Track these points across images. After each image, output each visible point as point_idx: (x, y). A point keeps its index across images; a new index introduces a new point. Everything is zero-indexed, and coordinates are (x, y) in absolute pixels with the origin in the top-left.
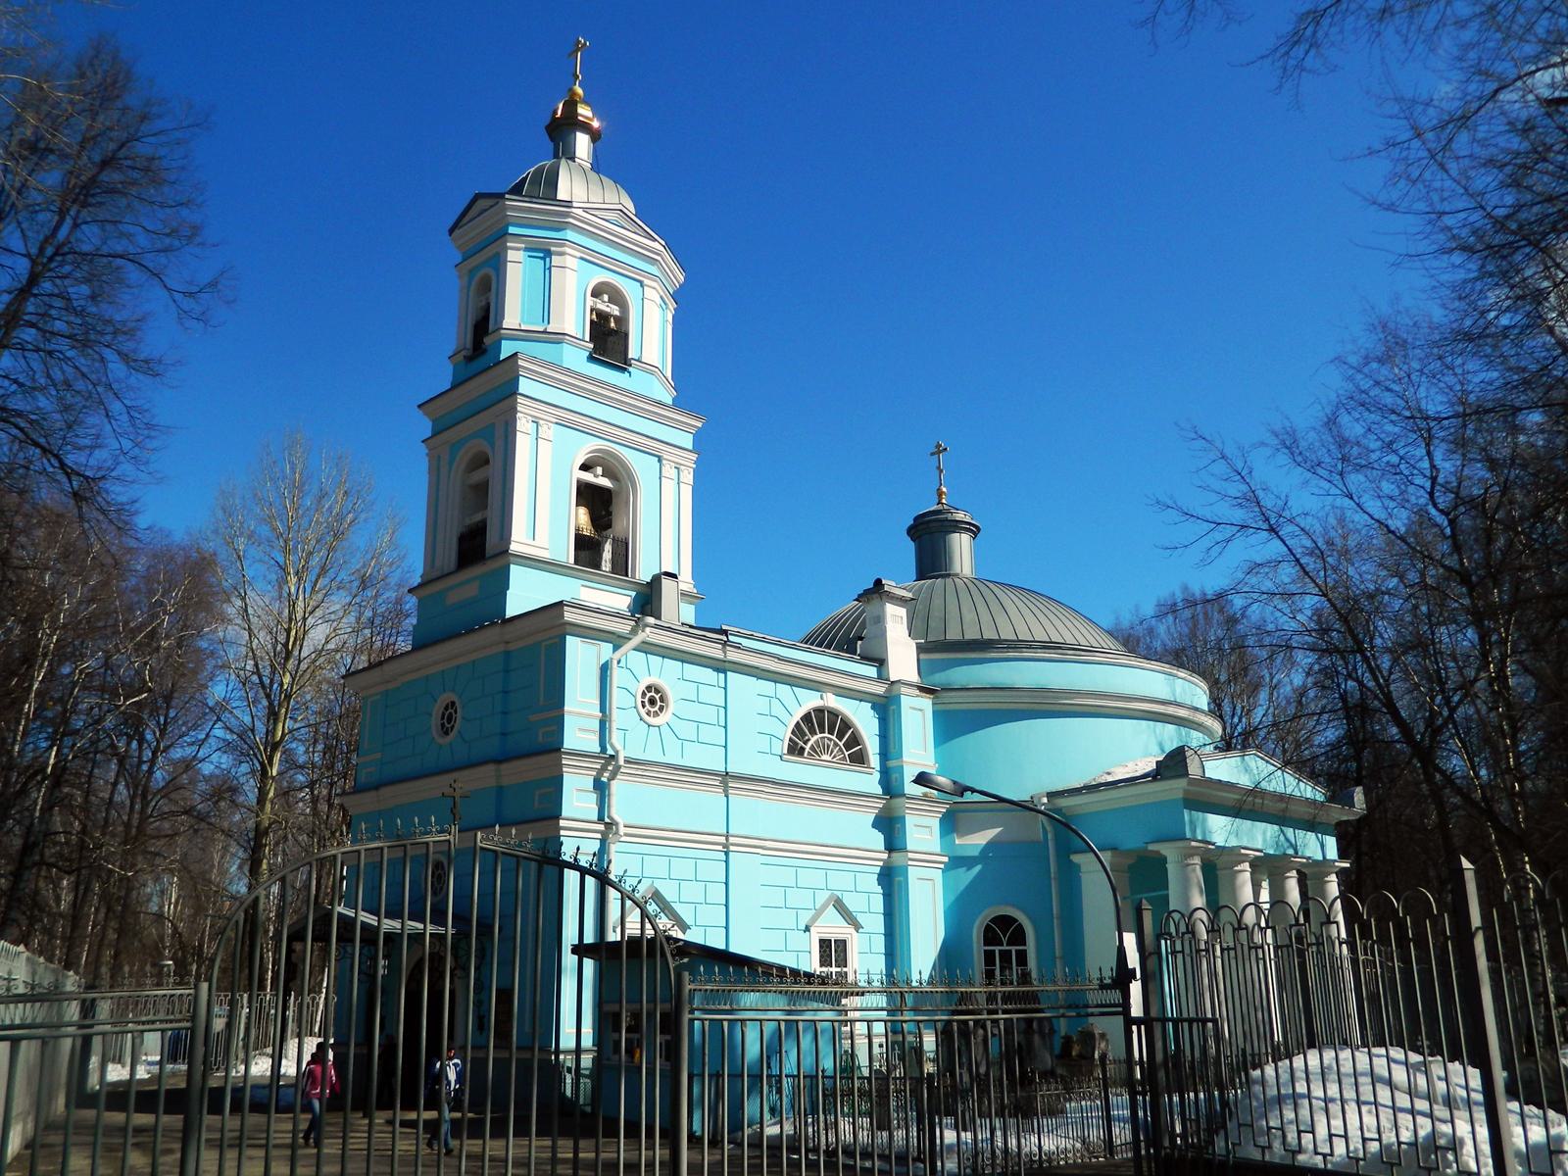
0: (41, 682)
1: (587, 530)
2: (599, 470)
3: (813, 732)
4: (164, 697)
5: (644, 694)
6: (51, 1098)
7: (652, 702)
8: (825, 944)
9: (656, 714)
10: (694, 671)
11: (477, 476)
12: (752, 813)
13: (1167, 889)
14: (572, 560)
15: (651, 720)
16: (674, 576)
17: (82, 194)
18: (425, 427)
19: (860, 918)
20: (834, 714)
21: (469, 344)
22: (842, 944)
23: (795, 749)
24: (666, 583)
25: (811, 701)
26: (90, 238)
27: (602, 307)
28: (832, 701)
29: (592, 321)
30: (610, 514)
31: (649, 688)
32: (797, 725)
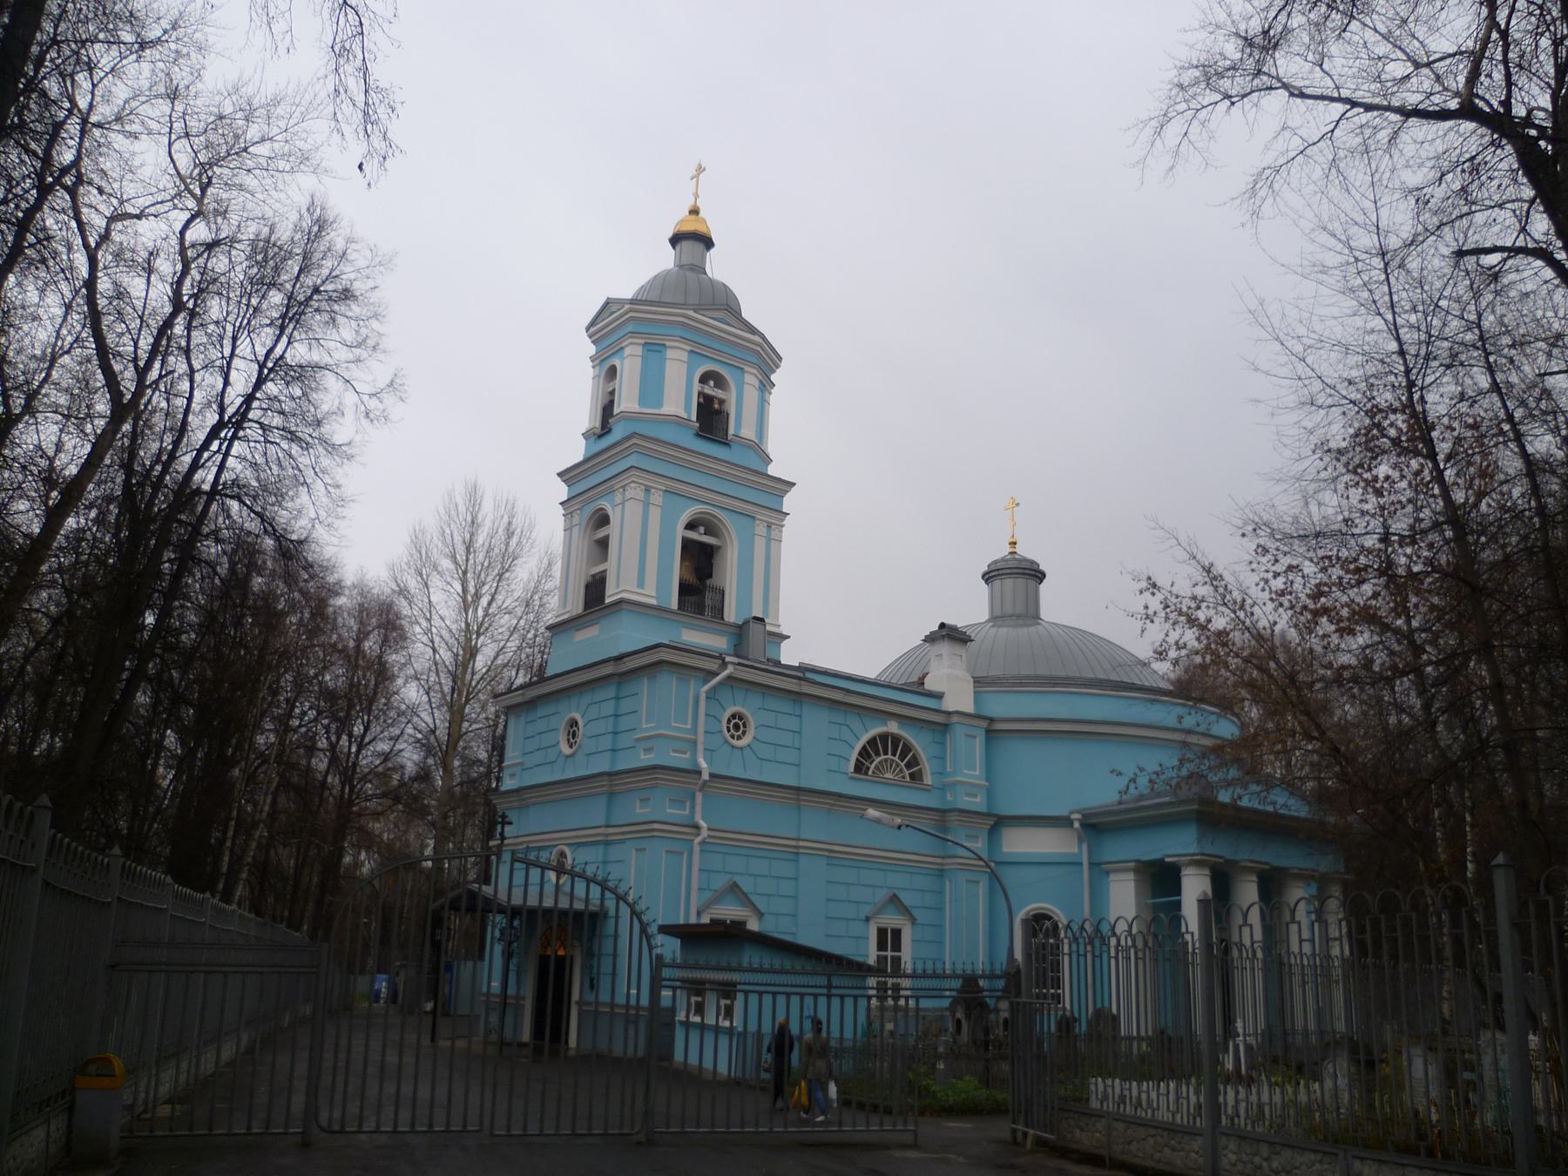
0: (229, 819)
1: (691, 578)
2: (702, 529)
3: (878, 754)
4: (366, 689)
5: (729, 721)
6: (876, 808)
7: (737, 727)
8: (882, 932)
9: (739, 738)
10: (773, 703)
11: (601, 534)
12: (815, 826)
13: (1179, 893)
14: (674, 605)
15: (735, 742)
16: (762, 620)
17: (292, 317)
18: (563, 492)
19: (915, 913)
20: (896, 740)
21: (598, 424)
22: (897, 933)
23: (860, 768)
24: (754, 626)
25: (876, 730)
26: (299, 353)
27: (708, 391)
28: (893, 727)
29: (699, 404)
30: (711, 565)
31: (734, 716)
32: (864, 748)
